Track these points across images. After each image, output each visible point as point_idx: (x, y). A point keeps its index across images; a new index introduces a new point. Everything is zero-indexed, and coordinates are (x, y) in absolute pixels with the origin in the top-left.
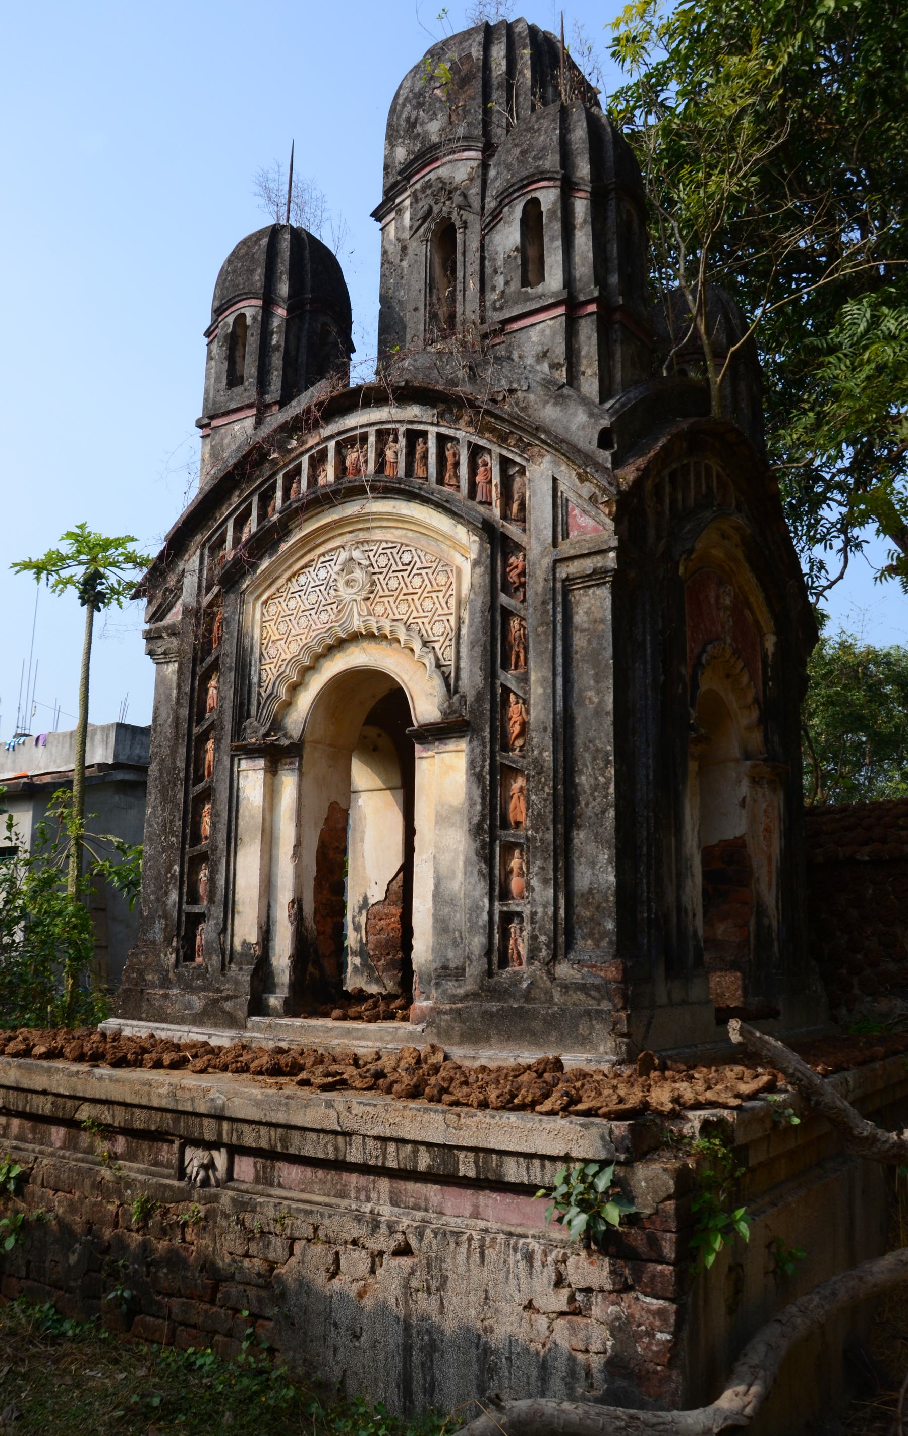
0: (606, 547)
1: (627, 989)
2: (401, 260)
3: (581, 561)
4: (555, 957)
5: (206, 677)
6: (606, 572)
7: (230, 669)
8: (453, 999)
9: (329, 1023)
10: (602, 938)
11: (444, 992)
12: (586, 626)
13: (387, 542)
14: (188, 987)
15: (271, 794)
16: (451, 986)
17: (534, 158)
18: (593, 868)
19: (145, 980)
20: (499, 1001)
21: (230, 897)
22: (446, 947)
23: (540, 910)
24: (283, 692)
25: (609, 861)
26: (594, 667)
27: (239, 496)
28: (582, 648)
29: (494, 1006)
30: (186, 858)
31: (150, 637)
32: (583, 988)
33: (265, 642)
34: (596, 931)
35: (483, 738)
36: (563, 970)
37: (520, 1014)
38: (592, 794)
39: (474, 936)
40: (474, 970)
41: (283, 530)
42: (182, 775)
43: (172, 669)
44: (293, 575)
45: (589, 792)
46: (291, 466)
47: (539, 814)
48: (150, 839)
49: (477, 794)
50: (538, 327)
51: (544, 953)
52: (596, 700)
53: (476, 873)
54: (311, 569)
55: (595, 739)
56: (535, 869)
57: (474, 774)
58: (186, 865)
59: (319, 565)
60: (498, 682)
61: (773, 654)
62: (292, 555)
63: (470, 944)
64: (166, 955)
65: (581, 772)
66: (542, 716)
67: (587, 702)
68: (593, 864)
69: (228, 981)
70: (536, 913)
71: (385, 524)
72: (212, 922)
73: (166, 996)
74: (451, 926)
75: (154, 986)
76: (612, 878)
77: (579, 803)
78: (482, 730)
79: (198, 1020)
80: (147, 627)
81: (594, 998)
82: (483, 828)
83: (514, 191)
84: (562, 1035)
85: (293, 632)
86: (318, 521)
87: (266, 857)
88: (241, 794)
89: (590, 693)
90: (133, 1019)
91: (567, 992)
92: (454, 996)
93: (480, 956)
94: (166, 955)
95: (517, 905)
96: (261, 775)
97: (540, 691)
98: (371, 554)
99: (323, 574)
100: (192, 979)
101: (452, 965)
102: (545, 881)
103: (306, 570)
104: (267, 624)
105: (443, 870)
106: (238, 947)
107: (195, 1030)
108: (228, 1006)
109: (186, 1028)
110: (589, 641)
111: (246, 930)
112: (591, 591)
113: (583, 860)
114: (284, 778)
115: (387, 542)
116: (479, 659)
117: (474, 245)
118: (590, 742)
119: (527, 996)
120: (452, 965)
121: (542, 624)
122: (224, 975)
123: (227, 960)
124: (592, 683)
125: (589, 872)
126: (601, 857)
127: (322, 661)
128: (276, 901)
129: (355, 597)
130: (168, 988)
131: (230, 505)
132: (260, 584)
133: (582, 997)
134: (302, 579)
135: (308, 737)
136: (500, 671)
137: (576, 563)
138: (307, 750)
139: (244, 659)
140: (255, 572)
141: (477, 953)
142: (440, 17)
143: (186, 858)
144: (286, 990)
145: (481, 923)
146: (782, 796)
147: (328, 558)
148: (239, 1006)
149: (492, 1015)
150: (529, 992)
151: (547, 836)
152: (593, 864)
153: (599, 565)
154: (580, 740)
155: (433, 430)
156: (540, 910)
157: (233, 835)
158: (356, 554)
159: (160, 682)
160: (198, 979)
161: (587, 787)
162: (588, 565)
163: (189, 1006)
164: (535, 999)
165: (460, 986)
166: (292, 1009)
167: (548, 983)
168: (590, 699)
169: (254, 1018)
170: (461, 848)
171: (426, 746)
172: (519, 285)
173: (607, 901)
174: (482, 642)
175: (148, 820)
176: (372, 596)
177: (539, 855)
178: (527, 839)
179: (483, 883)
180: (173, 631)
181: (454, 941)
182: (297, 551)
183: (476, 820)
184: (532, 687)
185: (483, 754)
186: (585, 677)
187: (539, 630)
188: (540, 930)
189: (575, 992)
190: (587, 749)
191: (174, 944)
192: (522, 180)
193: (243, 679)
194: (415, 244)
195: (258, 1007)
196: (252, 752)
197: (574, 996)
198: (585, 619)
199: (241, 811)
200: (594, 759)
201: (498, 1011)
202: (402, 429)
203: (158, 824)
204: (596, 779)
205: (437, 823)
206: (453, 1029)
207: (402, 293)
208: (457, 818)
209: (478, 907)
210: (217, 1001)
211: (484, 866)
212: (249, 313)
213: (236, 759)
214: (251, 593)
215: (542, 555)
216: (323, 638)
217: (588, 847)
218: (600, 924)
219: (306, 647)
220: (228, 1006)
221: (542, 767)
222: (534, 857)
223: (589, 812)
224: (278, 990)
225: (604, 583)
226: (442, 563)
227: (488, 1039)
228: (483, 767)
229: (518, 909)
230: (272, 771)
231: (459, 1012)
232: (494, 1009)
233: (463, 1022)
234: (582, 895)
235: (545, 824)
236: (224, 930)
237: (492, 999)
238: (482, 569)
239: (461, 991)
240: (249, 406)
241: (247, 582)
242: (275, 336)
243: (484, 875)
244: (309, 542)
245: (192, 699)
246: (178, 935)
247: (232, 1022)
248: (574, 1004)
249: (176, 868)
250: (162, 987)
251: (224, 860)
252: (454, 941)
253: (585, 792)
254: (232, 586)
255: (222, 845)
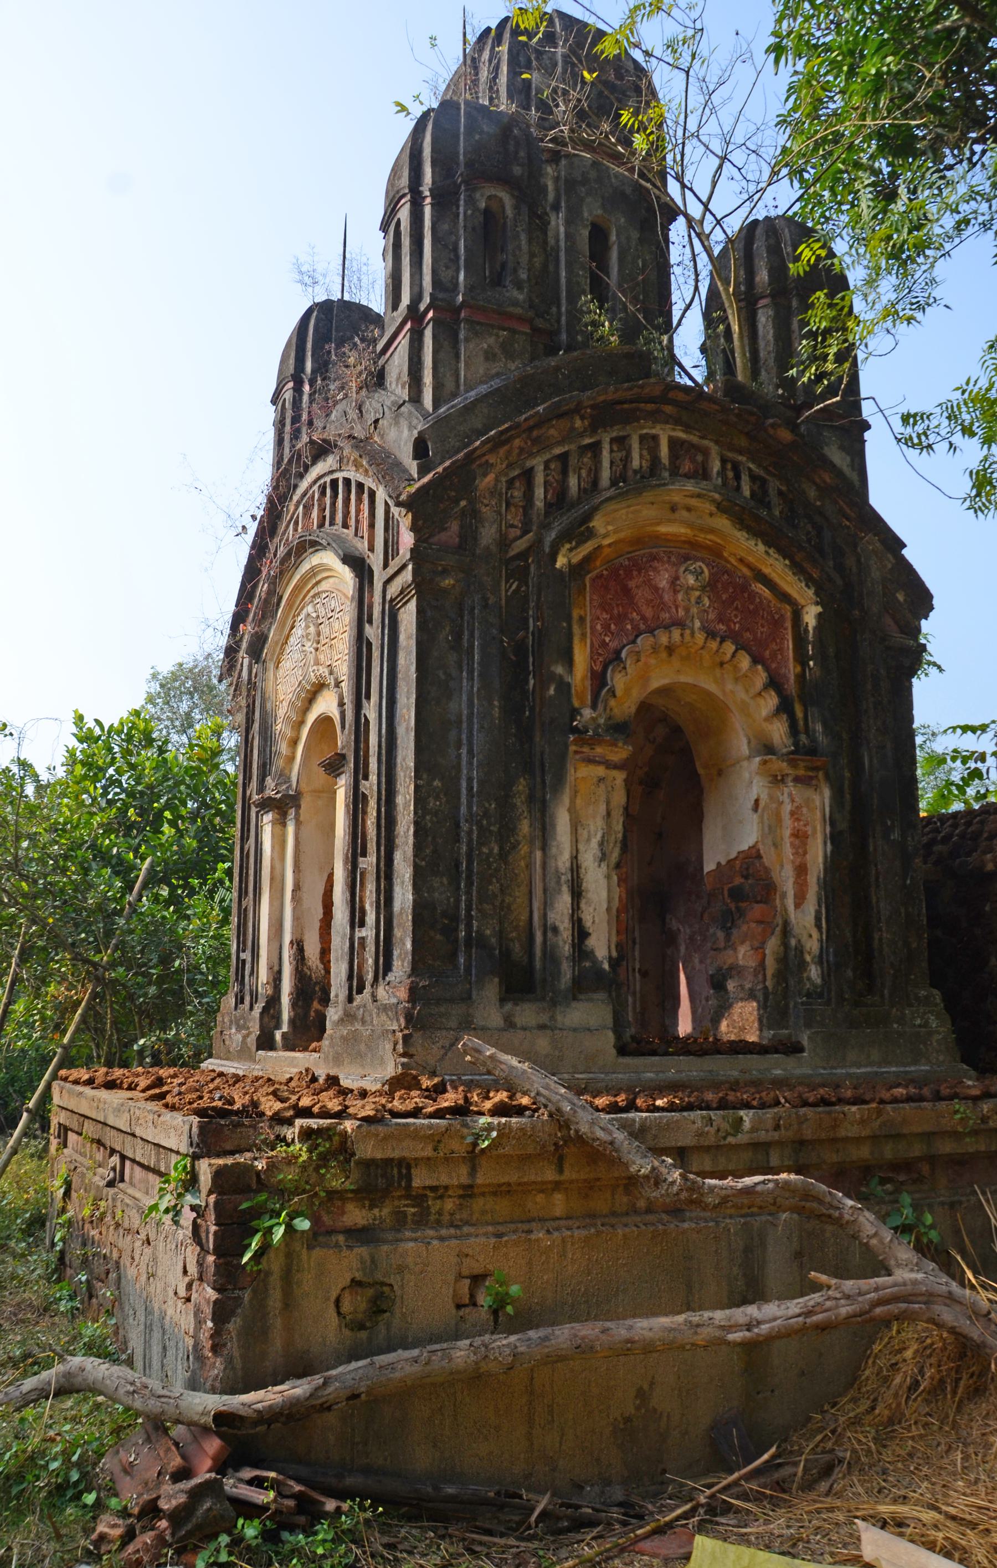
1: (414, 1008)
15: (280, 843)
61: (815, 628)
87: (277, 903)
135: (304, 787)
138: (305, 803)
142: (433, 46)
146: (827, 793)
166: (290, 1045)
195: (266, 1042)
230: (281, 822)
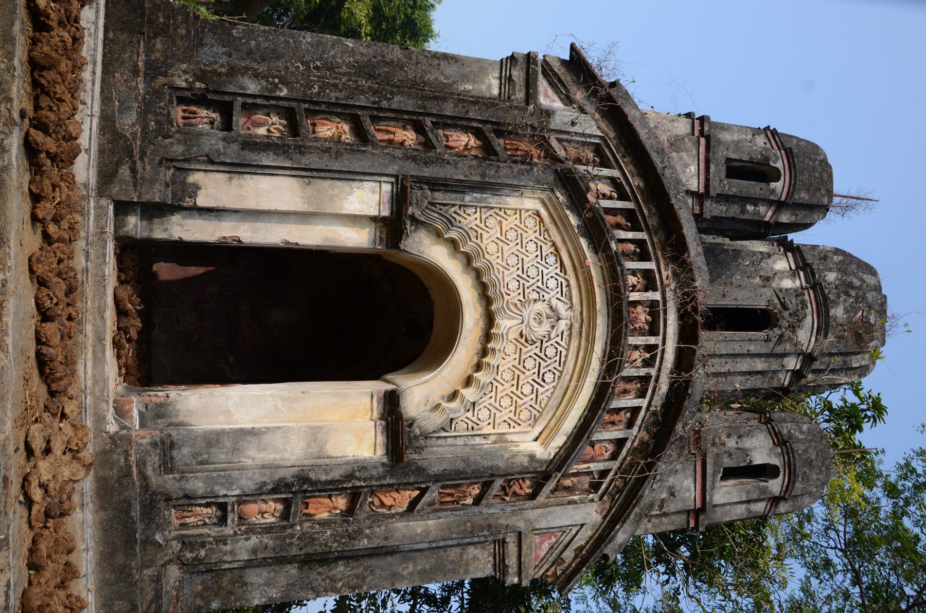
0: (523, 576)
2: (760, 276)
3: (516, 554)
4: (184, 565)
5: (478, 133)
6: (504, 575)
7: (483, 175)
8: (141, 464)
9: (111, 282)
10: (203, 599)
11: (148, 453)
12: (465, 557)
13: (566, 356)
14: (146, 109)
15: (354, 219)
16: (154, 459)
17: (805, 472)
18: (265, 585)
19: (155, 37)
20: (142, 513)
21: (248, 170)
22: (193, 445)
23: (228, 548)
24: (453, 234)
25: (271, 599)
26: (431, 568)
27: (638, 187)
28: (448, 556)
29: (136, 511)
30: (294, 104)
31: (529, 58)
32: (158, 596)
33: (502, 213)
34: (209, 593)
35: (384, 478)
36: (174, 572)
37: (130, 540)
38: (328, 577)
39: (204, 482)
40: (169, 483)
41: (599, 241)
42: (384, 104)
43: (492, 86)
44: (557, 250)
45: (330, 574)
46: (650, 249)
47: (314, 539)
48: (319, 43)
49: (336, 474)
50: (692, 485)
51: (189, 555)
52: (405, 573)
53: (263, 479)
54: (558, 271)
55: (373, 575)
56: (266, 539)
57: (354, 471)
58: (286, 104)
59: (560, 279)
60: (430, 484)
62: (575, 249)
63: (196, 478)
64: (185, 72)
65: (347, 566)
66: (398, 534)
67: (404, 565)
68: (268, 584)
69: (153, 168)
70: (225, 544)
71: (581, 354)
72: (221, 145)
73: (135, 72)
74: (213, 450)
75: (149, 50)
76: (256, 602)
77: (321, 566)
78: (392, 476)
79: (107, 123)
80: (540, 57)
81: (148, 608)
82: (304, 484)
83: (789, 457)
84: (112, 585)
85: (506, 248)
86: (602, 302)
88: (356, 184)
89: (411, 567)
90: (106, 16)
91: (154, 581)
92: (145, 464)
93: (184, 490)
94: (185, 72)
95: (233, 521)
96: (374, 212)
97: (419, 531)
98: (558, 339)
99: (552, 283)
100: (156, 114)
101: (175, 453)
102: (254, 551)
103: (558, 265)
104: (518, 216)
105: (266, 438)
106: (194, 178)
107: (96, 121)
108: (125, 171)
109: (97, 108)
110: (452, 562)
111: (213, 188)
112: (491, 559)
113: (272, 574)
114: (367, 230)
115: (566, 356)
116: (453, 467)
117: (753, 348)
118: (372, 571)
119: (148, 542)
120: (175, 453)
121: (473, 526)
122: (160, 163)
123: (178, 165)
124: (419, 568)
125: (261, 581)
126: (274, 591)
127: (473, 274)
128: (241, 220)
129: (526, 322)
130: (146, 74)
131: (633, 176)
132: (556, 209)
133: (149, 597)
134: (551, 260)
136: (440, 484)
137: (516, 549)
139: (488, 189)
140: (568, 208)
141: (187, 486)
143: (294, 104)
144: (145, 234)
145: (216, 488)
147: (564, 290)
148: (122, 188)
149: (127, 512)
150: (151, 544)
151: (295, 549)
152: (268, 584)
153: (510, 570)
154: (374, 562)
155: (644, 403)
156: (228, 548)
157: (315, 174)
158: (563, 325)
159: (481, 65)
160: (157, 122)
161: (334, 572)
162: (512, 561)
163: (124, 109)
164: (145, 550)
165: (154, 470)
167: (161, 562)
168: (407, 568)
169: (111, 207)
170: (286, 455)
171: (382, 401)
172: (726, 466)
173: (236, 600)
174: (467, 469)
175: (340, 42)
176: (523, 341)
177: (278, 542)
178: (292, 526)
179: (253, 488)
180: (530, 94)
181: (199, 454)
182: (577, 254)
183: (312, 476)
184: (423, 522)
185: (370, 479)
186: (425, 561)
187: (469, 524)
188: (211, 549)
189: (154, 589)
190: (366, 569)
191: (198, 85)
192: (795, 465)
193: (470, 187)
194: (769, 294)
195: (122, 208)
196: (399, 200)
197: (149, 589)
198: (471, 556)
199: (339, 183)
200: (357, 576)
201: (132, 518)
202: (653, 372)
203: (334, 57)
204: (341, 580)
205: (312, 428)
206: (111, 469)
207: (738, 277)
208: (314, 450)
209: (232, 483)
210: (131, 156)
211: (270, 487)
212: (777, 186)
213: (393, 180)
214: (550, 199)
215: (528, 521)
216: (495, 286)
217: (283, 579)
218: (216, 596)
219: (490, 267)
220: (125, 171)
221: (354, 538)
222: (277, 538)
223: (313, 576)
224: (145, 223)
225: (495, 570)
226: (538, 414)
227: (103, 508)
228: (359, 479)
229: (229, 522)
231: (129, 475)
232: (133, 514)
233: (119, 480)
234: (241, 577)
235: (306, 546)
236: (211, 162)
237: (143, 506)
238: (526, 464)
239: (149, 471)
240: (707, 186)
241: (561, 198)
242: (753, 208)
243: (261, 488)
244: (580, 266)
245: (461, 119)
246: (207, 90)
247: (106, 177)
248: (142, 590)
249: (284, 92)
250: (147, 63)
251: (288, 164)
252: (199, 454)
253: (329, 571)
254: (561, 180)
255: (305, 161)
